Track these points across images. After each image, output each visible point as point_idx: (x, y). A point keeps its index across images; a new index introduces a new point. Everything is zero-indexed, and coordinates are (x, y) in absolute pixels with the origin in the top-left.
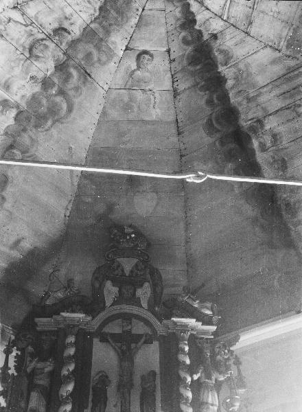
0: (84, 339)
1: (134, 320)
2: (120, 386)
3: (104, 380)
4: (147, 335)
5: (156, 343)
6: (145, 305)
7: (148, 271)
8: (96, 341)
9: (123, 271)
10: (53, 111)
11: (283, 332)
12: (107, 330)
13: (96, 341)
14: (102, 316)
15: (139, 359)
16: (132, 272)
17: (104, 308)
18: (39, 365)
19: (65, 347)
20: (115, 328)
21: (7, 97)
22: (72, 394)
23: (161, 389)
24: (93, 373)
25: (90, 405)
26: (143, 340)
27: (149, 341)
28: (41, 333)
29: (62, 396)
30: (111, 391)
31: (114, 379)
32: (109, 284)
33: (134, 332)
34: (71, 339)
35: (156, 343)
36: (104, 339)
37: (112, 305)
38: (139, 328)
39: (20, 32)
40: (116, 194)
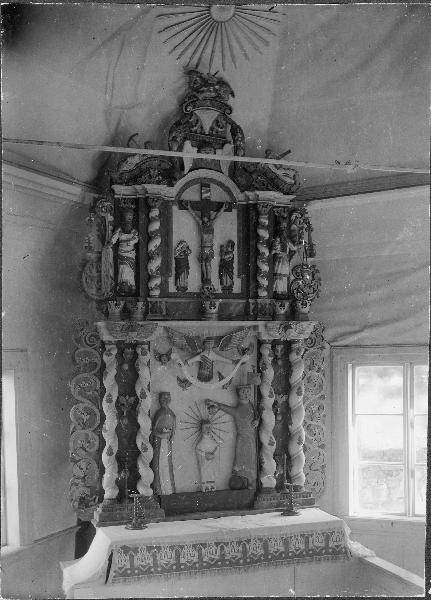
0: (166, 207)
3: (186, 252)
5: (235, 211)
7: (229, 127)
8: (175, 208)
9: (202, 128)
13: (175, 208)
14: (180, 184)
16: (212, 129)
18: (124, 237)
19: (149, 221)
20: (192, 195)
21: (210, 524)
22: (159, 269)
24: (174, 244)
25: (174, 272)
26: (224, 208)
27: (229, 210)
28: (303, 212)
29: (151, 270)
31: (194, 246)
33: (213, 199)
35: (235, 211)
36: (183, 205)
37: (191, 170)
40: (92, 256)
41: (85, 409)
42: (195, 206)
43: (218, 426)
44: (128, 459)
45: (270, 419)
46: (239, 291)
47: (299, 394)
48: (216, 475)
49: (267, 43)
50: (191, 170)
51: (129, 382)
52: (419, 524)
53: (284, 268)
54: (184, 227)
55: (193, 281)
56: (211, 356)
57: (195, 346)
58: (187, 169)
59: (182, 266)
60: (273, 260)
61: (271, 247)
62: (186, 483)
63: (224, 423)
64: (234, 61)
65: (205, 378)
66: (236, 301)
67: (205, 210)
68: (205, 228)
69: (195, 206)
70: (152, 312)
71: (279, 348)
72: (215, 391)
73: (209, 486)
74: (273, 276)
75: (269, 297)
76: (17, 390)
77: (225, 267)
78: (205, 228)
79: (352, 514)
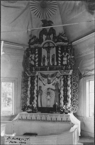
1: (50, 43)
2: (47, 58)
3: (44, 57)
4: (53, 46)
6: (52, 40)
8: (43, 49)
10: (26, 58)
11: (34, 114)
12: (45, 46)
13: (43, 49)
14: (43, 43)
15: (51, 51)
17: (43, 42)
18: (32, 55)
19: (36, 51)
23: (71, 23)
26: (52, 48)
27: (53, 47)
30: (46, 59)
31: (46, 56)
32: (44, 35)
34: (37, 50)
37: (45, 40)
38: (51, 45)
39: (13, 17)
41: (25, 89)
42: (46, 48)
43: (51, 94)
44: (32, 99)
45: (62, 92)
46: (56, 65)
47: (69, 87)
48: (51, 104)
49: (56, 10)
50: (45, 40)
51: (32, 83)
52: (72, 142)
53: (65, 59)
54: (44, 52)
55: (46, 64)
56: (49, 78)
57: (45, 76)
58: (44, 41)
59: (44, 60)
60: (62, 57)
61: (61, 54)
62: (44, 106)
63: (53, 93)
64: (51, 15)
65: (49, 83)
66: (55, 67)
67: (48, 49)
68: (48, 52)
69: (46, 48)
70: (36, 70)
71: (65, 77)
72: (51, 86)
73: (49, 106)
74: (62, 61)
75: (61, 65)
76: (14, 84)
77: (53, 60)
78: (48, 52)
79: (80, 121)
